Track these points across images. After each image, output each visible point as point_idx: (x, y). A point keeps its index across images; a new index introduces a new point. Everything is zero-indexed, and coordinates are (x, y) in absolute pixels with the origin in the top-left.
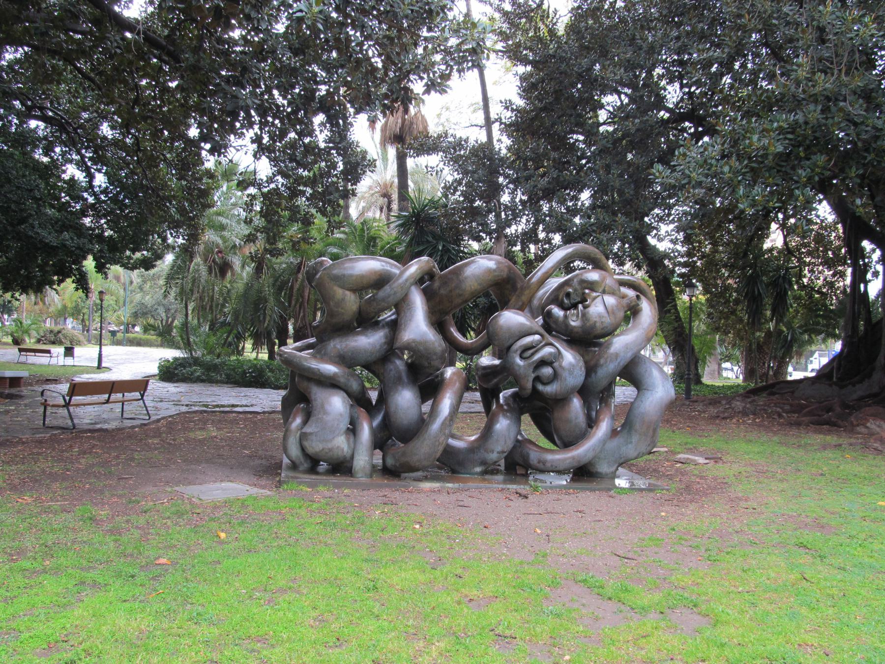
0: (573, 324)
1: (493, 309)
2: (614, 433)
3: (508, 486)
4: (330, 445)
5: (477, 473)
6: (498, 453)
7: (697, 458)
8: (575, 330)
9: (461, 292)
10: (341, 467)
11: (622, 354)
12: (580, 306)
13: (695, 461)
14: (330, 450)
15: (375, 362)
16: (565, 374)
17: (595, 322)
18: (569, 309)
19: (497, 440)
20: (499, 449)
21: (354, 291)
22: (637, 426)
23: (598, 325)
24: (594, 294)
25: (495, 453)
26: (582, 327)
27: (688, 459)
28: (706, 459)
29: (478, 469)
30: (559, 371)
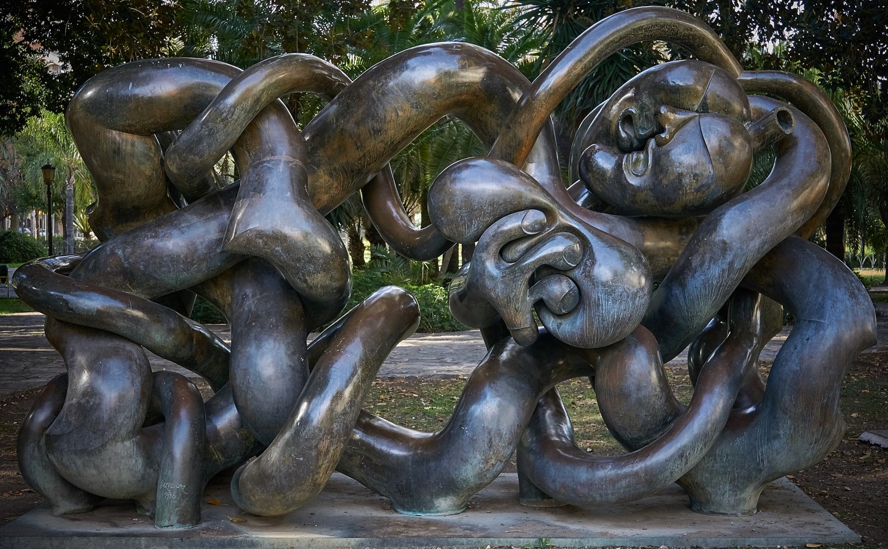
0: (633, 181)
1: (450, 156)
2: (733, 422)
8: (642, 196)
11: (736, 245)
12: (652, 143)
15: (213, 280)
16: (597, 294)
17: (681, 175)
18: (629, 150)
19: (473, 441)
21: (144, 132)
23: (686, 181)
24: (679, 117)
26: (655, 187)
30: (586, 284)
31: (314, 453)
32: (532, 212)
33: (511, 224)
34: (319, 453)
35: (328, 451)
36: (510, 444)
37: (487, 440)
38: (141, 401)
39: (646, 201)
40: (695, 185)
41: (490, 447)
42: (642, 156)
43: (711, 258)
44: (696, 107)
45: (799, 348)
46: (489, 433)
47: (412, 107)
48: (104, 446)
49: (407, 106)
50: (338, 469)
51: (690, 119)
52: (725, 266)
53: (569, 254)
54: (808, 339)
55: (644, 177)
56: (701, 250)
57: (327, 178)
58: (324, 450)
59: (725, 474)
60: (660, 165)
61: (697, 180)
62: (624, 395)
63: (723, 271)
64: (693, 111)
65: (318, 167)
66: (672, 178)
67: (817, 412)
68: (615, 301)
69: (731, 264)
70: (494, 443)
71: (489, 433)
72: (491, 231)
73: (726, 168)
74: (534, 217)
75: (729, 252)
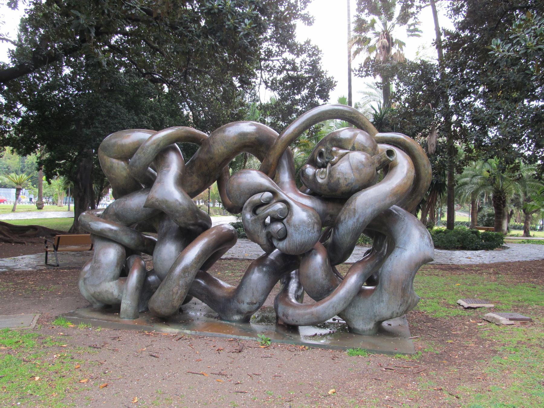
0: (320, 181)
3: (241, 337)
4: (98, 290)
5: (235, 321)
6: (248, 303)
7: (501, 318)
9: (211, 156)
10: (111, 307)
13: (498, 320)
14: (100, 293)
17: (339, 179)
20: (248, 300)
22: (386, 284)
23: (341, 181)
24: (341, 151)
25: (245, 304)
26: (328, 183)
27: (494, 318)
28: (510, 319)
29: (237, 317)
31: (171, 293)
32: (266, 193)
33: (257, 197)
34: (173, 293)
35: (177, 293)
36: (263, 295)
38: (117, 266)
39: (325, 190)
40: (345, 183)
41: (253, 296)
42: (325, 170)
44: (350, 148)
48: (101, 283)
50: (339, 315)
51: (347, 153)
52: (355, 220)
53: (281, 211)
55: (325, 180)
56: (345, 213)
57: (196, 178)
60: (331, 175)
62: (308, 277)
65: (193, 173)
66: (335, 179)
67: (399, 291)
68: (299, 234)
69: (358, 219)
72: (248, 201)
74: (268, 194)
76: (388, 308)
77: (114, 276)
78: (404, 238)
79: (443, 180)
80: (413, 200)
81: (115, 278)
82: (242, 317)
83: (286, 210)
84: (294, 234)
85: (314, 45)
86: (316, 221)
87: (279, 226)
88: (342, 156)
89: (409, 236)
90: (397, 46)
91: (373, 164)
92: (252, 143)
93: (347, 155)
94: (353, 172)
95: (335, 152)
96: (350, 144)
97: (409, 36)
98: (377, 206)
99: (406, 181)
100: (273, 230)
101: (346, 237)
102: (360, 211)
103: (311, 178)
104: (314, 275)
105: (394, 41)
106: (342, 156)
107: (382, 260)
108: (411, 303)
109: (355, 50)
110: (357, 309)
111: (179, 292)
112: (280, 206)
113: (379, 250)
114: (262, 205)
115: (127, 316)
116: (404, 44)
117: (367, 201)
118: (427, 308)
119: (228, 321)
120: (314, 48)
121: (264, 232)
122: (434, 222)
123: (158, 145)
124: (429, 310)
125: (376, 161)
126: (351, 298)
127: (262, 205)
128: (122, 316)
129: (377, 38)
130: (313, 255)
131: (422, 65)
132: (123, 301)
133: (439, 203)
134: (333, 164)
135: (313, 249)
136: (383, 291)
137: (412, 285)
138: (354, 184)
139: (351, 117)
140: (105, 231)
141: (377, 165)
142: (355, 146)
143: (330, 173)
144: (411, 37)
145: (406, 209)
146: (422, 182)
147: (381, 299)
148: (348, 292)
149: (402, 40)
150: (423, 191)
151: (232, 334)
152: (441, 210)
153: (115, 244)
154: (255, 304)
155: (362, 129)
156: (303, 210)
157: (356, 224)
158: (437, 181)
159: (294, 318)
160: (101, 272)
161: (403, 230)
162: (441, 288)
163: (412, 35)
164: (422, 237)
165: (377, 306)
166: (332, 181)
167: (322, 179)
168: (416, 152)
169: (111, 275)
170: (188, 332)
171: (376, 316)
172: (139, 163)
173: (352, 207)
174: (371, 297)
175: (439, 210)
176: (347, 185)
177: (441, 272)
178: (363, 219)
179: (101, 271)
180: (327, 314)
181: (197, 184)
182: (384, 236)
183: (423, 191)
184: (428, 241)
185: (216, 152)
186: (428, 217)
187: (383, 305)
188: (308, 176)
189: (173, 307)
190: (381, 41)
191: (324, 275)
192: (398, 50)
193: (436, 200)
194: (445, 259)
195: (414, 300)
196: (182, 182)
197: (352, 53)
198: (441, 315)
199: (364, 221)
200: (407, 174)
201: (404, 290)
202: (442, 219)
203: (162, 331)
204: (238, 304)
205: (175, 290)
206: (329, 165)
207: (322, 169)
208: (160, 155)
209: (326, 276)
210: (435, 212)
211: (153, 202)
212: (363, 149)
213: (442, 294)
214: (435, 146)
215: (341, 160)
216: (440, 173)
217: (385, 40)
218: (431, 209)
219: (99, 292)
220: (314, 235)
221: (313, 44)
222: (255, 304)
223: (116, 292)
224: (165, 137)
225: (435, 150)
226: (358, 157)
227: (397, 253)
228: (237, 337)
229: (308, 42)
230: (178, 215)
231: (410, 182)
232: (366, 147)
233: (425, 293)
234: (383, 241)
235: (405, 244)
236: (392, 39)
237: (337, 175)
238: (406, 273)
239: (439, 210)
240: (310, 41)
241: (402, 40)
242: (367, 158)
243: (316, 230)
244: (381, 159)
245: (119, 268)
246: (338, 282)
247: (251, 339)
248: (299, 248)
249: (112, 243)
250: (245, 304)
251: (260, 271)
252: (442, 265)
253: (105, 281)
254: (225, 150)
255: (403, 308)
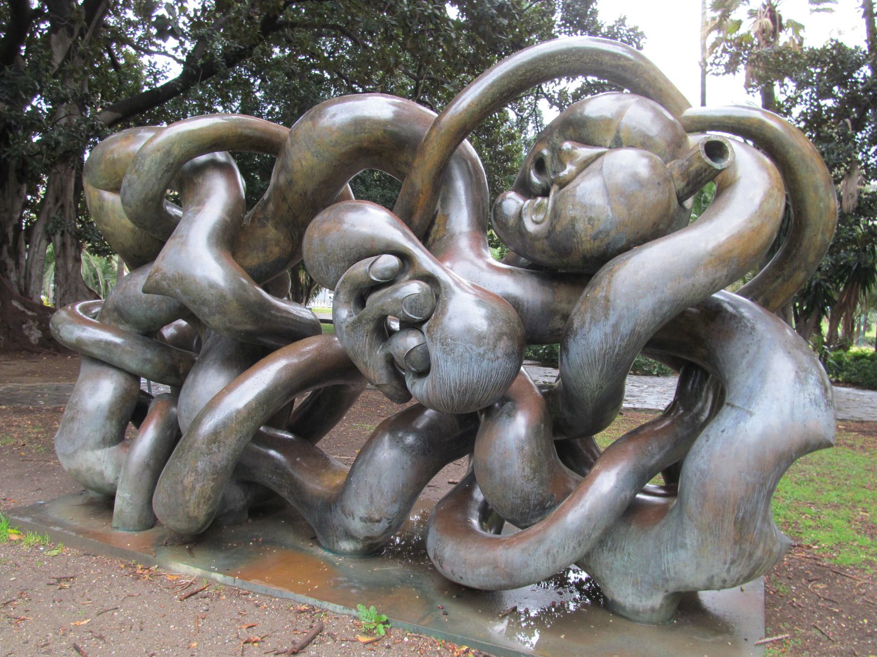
0: (530, 227)
3: (326, 605)
5: (343, 553)
8: (538, 245)
17: (573, 220)
23: (580, 226)
24: (584, 152)
25: (357, 519)
26: (550, 233)
29: (346, 546)
31: (180, 488)
34: (185, 489)
35: (194, 488)
37: (368, 496)
39: (544, 252)
40: (590, 232)
41: (372, 502)
42: (546, 200)
43: (592, 318)
44: (608, 143)
45: (710, 441)
46: (371, 488)
47: (313, 156)
48: (75, 452)
49: (308, 155)
51: (599, 155)
52: (608, 329)
53: (414, 302)
54: (723, 431)
55: (543, 225)
58: (190, 486)
59: (626, 574)
61: (593, 225)
63: (606, 335)
64: (605, 147)
65: (267, 221)
66: (564, 223)
67: (729, 527)
68: (454, 361)
69: (615, 326)
70: (375, 500)
71: (371, 488)
73: (629, 210)
74: (389, 261)
75: (611, 312)
76: (698, 565)
77: (104, 439)
78: (750, 382)
79: (870, 261)
80: (785, 281)
81: (106, 442)
82: (359, 546)
83: (431, 301)
84: (441, 362)
85: (632, 26)
86: (505, 329)
87: (412, 341)
88: (587, 163)
89: (763, 376)
90: (790, 29)
91: (668, 179)
92: (378, 142)
93: (599, 160)
94: (609, 203)
95: (570, 155)
96: (608, 130)
97: (812, 11)
98: (668, 292)
99: (757, 223)
100: (396, 351)
101: (587, 374)
102: (620, 303)
103: (511, 222)
104: (503, 467)
105: (784, 22)
106: (587, 163)
107: (696, 429)
108: (762, 558)
109: (713, 40)
110: (619, 556)
111: (198, 487)
112: (413, 288)
113: (688, 409)
114: (376, 287)
115: (124, 524)
116: (802, 27)
117: (647, 278)
118: (822, 535)
119: (330, 550)
120: (632, 30)
121: (379, 354)
122: (852, 340)
123: (168, 153)
124: (825, 539)
125: (676, 173)
126: (596, 534)
127: (376, 287)
128: (115, 524)
129: (754, 19)
130: (504, 416)
131: (834, 48)
132: (118, 492)
133: (862, 304)
134: (563, 184)
135: (505, 399)
136: (686, 520)
137: (766, 510)
138: (612, 233)
139: (617, 67)
140: (86, 344)
141: (680, 184)
142: (622, 135)
143: (554, 209)
144: (816, 13)
145: (765, 304)
146: (808, 233)
147: (679, 539)
148: (589, 518)
149: (799, 21)
150: (811, 258)
151: (309, 595)
152: (866, 319)
153: (112, 371)
154: (379, 521)
155: (647, 95)
156: (480, 303)
157: (610, 340)
158: (859, 264)
159: (455, 570)
160: (76, 429)
161: (748, 357)
162: (858, 481)
163: (818, 10)
164: (801, 377)
165: (671, 555)
166: (558, 228)
167: (537, 223)
168: (793, 153)
169: (98, 437)
170: (219, 577)
171: (667, 580)
172: (132, 196)
173: (599, 293)
174: (657, 528)
175: (862, 318)
176: (595, 238)
177: (860, 440)
178: (631, 326)
179: (76, 426)
180: (531, 569)
181: (277, 245)
182: (706, 374)
183: (811, 258)
184: (818, 391)
185: (297, 167)
186: (840, 331)
187: (687, 557)
188: (506, 217)
189: (191, 519)
190: (759, 21)
191: (527, 470)
192: (791, 38)
193: (856, 299)
194: (870, 410)
195: (771, 551)
196: (231, 238)
197: (708, 47)
198: (853, 559)
199: (633, 330)
200: (761, 205)
201: (742, 525)
202: (867, 334)
203: (169, 569)
204: (344, 517)
205: (188, 480)
206: (554, 189)
207: (539, 199)
208: (183, 176)
209: (535, 471)
210: (853, 321)
211: (157, 282)
212: (643, 143)
213: (861, 496)
214: (856, 197)
215: (584, 172)
216: (864, 250)
217: (768, 20)
218: (846, 319)
219: (75, 470)
220: (496, 364)
221: (630, 24)
222: (379, 521)
223: (109, 473)
224: (182, 137)
225: (856, 205)
226: (629, 163)
227: (727, 419)
228: (317, 603)
229: (622, 21)
230: (206, 310)
231: (770, 228)
232: (649, 138)
233: (819, 491)
234: (701, 383)
235: (750, 398)
236: (780, 19)
237: (570, 212)
238: (749, 479)
239: (862, 318)
240: (625, 18)
241: (799, 21)
242: (653, 167)
243: (500, 352)
244: (690, 165)
245: (114, 422)
246: (572, 486)
247: (347, 611)
248: (456, 397)
249: (105, 369)
250: (357, 519)
251: (397, 442)
252: (863, 422)
253: (84, 446)
254: (315, 160)
255: (738, 571)
